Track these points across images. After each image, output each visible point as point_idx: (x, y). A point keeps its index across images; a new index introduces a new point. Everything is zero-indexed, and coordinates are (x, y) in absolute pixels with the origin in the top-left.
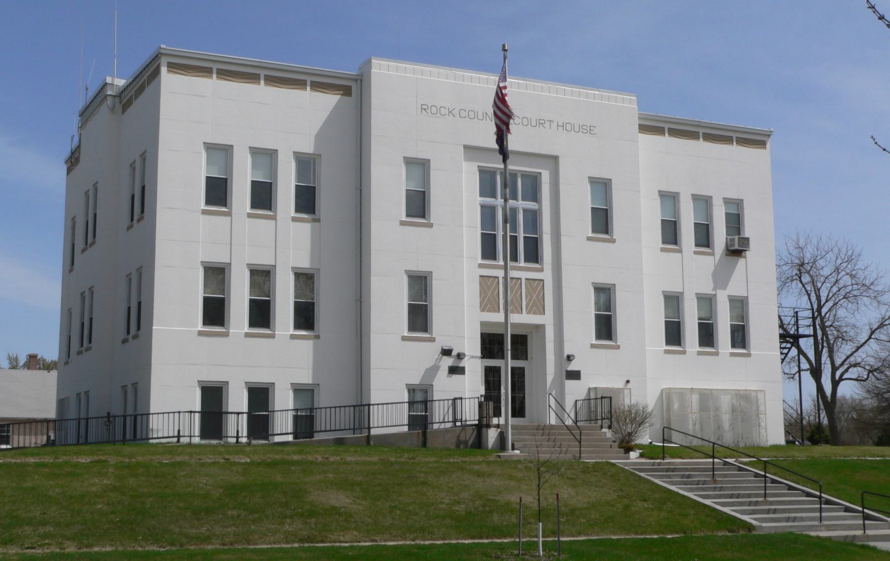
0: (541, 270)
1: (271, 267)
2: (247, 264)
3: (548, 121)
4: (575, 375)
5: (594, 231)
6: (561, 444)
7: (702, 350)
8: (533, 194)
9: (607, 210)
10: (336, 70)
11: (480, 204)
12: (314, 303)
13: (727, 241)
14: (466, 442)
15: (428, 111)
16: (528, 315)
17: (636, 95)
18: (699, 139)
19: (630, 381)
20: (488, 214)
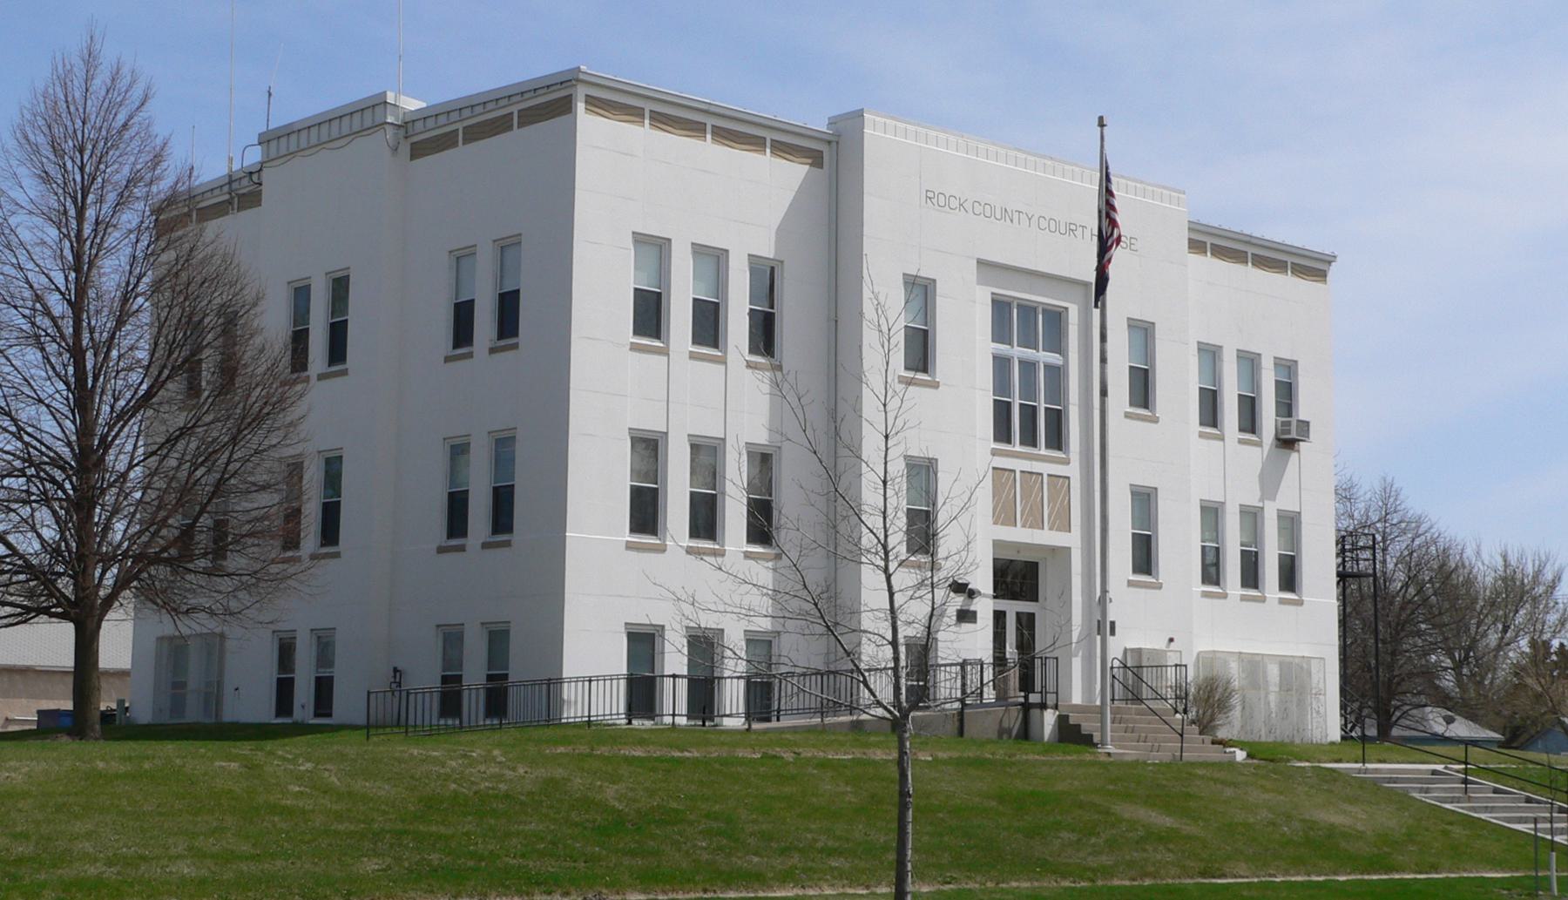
0: (1067, 462)
1: (717, 442)
5: (1131, 404)
6: (1146, 737)
8: (1056, 341)
9: (1146, 370)
13: (1276, 425)
14: (1009, 731)
15: (935, 201)
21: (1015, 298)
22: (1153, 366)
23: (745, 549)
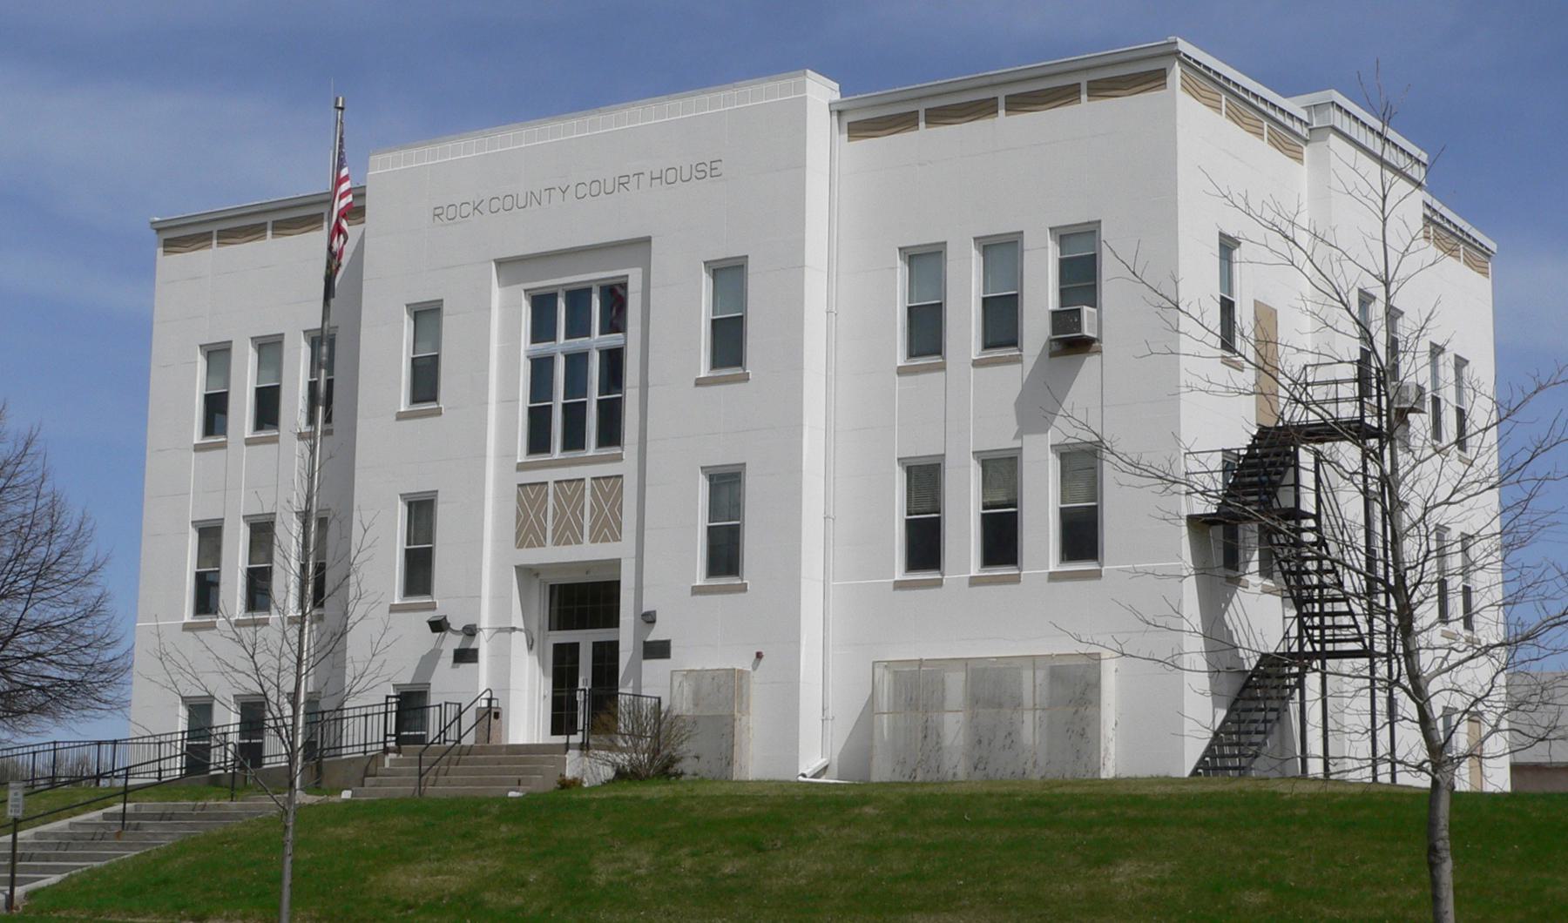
0: (619, 458)
3: (546, 190)
11: (528, 357)
16: (593, 545)
20: (541, 369)
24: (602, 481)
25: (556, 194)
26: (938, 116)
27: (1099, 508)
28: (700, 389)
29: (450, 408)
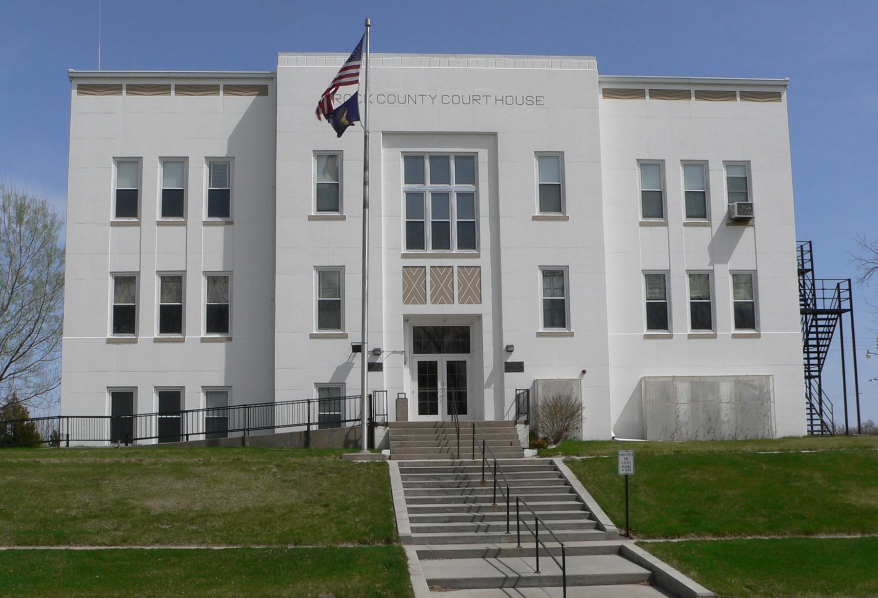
0: (478, 256)
2: (642, 270)
4: (517, 367)
7: (695, 333)
10: (657, 76)
12: (228, 305)
16: (434, 305)
17: (595, 57)
18: (690, 98)
19: (586, 371)
20: (414, 201)
21: (425, 152)
22: (564, 182)
23: (733, 332)
24: (410, 268)
25: (428, 100)
26: (656, 94)
27: (183, 306)
28: (535, 222)
29: (351, 217)
